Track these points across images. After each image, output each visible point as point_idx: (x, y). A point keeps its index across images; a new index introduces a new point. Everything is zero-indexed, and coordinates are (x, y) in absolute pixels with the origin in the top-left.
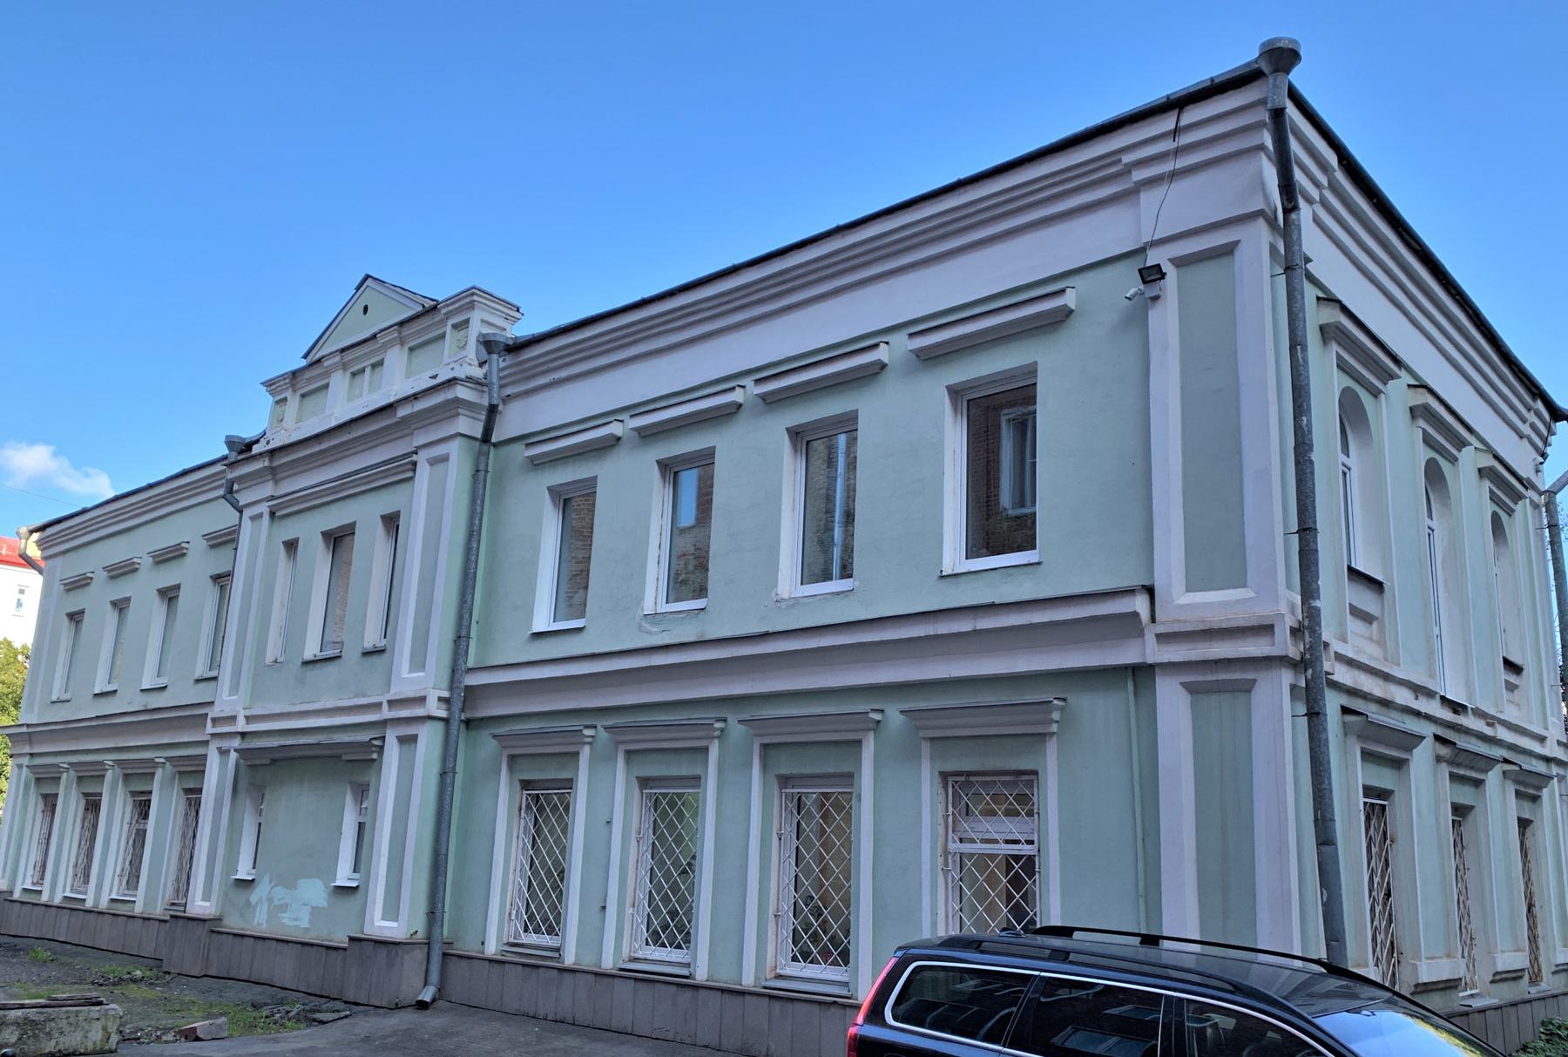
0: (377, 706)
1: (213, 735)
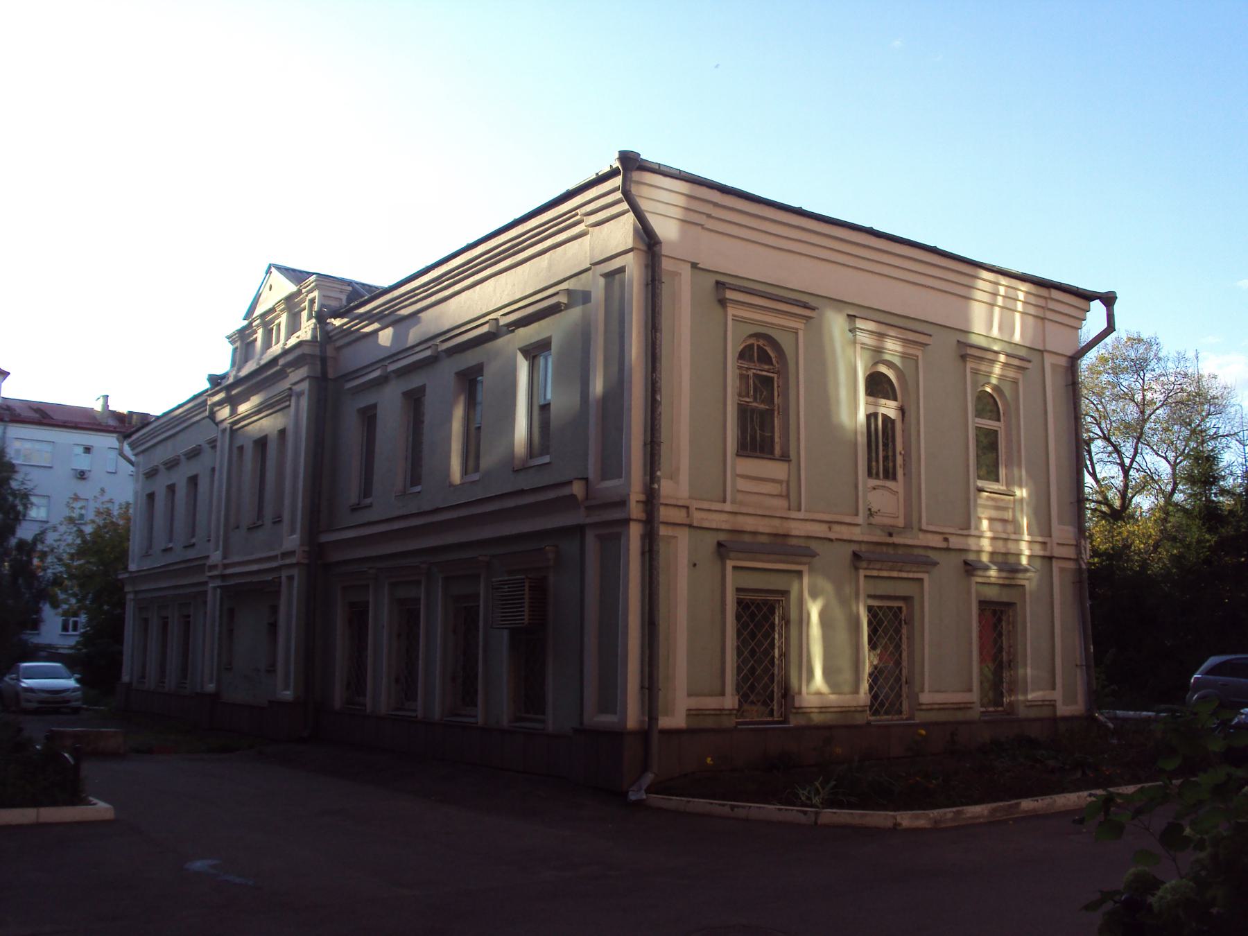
0: (274, 558)
1: (211, 577)
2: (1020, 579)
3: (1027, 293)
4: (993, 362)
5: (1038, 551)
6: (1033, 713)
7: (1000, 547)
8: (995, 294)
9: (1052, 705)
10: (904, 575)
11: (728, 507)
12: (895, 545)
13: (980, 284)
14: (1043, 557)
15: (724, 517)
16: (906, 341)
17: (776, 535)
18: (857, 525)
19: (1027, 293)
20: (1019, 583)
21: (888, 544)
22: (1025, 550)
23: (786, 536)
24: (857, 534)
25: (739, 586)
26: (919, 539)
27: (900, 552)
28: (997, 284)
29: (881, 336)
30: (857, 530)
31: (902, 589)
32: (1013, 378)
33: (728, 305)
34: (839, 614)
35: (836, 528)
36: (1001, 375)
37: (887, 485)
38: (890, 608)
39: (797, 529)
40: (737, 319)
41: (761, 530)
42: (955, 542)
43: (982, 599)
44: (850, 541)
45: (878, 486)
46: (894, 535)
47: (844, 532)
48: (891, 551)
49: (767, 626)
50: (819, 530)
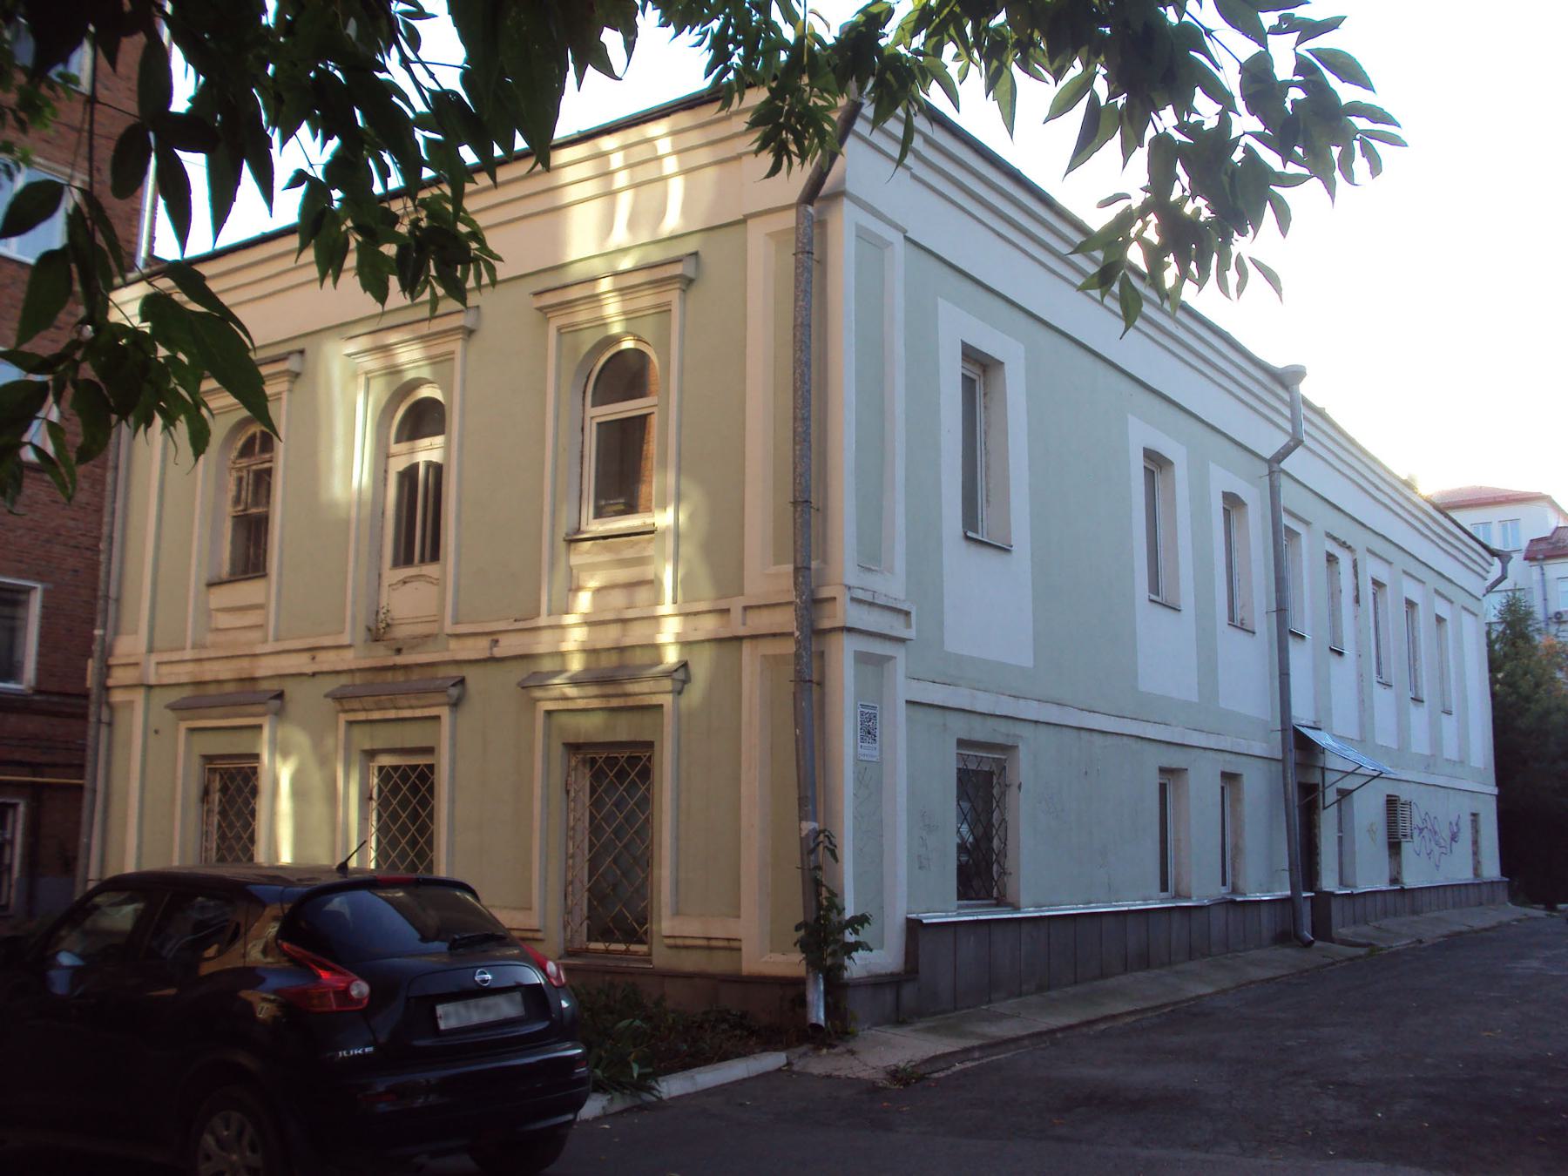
2: (596, 697)
3: (674, 133)
4: (595, 298)
5: (708, 626)
6: (690, 962)
7: (610, 636)
8: (607, 174)
9: (732, 947)
10: (407, 713)
11: (189, 654)
12: (406, 667)
13: (568, 175)
14: (719, 641)
15: (190, 667)
16: (422, 338)
17: (241, 680)
18: (349, 646)
19: (674, 133)
20: (646, 703)
21: (394, 668)
22: (669, 632)
23: (253, 679)
24: (348, 660)
25: (908, 699)
26: (448, 650)
27: (415, 676)
28: (602, 155)
29: (385, 349)
30: (349, 654)
31: (412, 736)
32: (386, 368)
33: (205, 399)
34: (316, 778)
35: (321, 656)
36: (624, 313)
37: (423, 572)
38: (414, 768)
39: (265, 668)
40: (438, 359)
41: (222, 676)
42: (509, 645)
43: (572, 740)
44: (337, 673)
45: (412, 577)
46: (404, 651)
47: (328, 661)
48: (400, 677)
49: (633, 774)
50: (300, 663)
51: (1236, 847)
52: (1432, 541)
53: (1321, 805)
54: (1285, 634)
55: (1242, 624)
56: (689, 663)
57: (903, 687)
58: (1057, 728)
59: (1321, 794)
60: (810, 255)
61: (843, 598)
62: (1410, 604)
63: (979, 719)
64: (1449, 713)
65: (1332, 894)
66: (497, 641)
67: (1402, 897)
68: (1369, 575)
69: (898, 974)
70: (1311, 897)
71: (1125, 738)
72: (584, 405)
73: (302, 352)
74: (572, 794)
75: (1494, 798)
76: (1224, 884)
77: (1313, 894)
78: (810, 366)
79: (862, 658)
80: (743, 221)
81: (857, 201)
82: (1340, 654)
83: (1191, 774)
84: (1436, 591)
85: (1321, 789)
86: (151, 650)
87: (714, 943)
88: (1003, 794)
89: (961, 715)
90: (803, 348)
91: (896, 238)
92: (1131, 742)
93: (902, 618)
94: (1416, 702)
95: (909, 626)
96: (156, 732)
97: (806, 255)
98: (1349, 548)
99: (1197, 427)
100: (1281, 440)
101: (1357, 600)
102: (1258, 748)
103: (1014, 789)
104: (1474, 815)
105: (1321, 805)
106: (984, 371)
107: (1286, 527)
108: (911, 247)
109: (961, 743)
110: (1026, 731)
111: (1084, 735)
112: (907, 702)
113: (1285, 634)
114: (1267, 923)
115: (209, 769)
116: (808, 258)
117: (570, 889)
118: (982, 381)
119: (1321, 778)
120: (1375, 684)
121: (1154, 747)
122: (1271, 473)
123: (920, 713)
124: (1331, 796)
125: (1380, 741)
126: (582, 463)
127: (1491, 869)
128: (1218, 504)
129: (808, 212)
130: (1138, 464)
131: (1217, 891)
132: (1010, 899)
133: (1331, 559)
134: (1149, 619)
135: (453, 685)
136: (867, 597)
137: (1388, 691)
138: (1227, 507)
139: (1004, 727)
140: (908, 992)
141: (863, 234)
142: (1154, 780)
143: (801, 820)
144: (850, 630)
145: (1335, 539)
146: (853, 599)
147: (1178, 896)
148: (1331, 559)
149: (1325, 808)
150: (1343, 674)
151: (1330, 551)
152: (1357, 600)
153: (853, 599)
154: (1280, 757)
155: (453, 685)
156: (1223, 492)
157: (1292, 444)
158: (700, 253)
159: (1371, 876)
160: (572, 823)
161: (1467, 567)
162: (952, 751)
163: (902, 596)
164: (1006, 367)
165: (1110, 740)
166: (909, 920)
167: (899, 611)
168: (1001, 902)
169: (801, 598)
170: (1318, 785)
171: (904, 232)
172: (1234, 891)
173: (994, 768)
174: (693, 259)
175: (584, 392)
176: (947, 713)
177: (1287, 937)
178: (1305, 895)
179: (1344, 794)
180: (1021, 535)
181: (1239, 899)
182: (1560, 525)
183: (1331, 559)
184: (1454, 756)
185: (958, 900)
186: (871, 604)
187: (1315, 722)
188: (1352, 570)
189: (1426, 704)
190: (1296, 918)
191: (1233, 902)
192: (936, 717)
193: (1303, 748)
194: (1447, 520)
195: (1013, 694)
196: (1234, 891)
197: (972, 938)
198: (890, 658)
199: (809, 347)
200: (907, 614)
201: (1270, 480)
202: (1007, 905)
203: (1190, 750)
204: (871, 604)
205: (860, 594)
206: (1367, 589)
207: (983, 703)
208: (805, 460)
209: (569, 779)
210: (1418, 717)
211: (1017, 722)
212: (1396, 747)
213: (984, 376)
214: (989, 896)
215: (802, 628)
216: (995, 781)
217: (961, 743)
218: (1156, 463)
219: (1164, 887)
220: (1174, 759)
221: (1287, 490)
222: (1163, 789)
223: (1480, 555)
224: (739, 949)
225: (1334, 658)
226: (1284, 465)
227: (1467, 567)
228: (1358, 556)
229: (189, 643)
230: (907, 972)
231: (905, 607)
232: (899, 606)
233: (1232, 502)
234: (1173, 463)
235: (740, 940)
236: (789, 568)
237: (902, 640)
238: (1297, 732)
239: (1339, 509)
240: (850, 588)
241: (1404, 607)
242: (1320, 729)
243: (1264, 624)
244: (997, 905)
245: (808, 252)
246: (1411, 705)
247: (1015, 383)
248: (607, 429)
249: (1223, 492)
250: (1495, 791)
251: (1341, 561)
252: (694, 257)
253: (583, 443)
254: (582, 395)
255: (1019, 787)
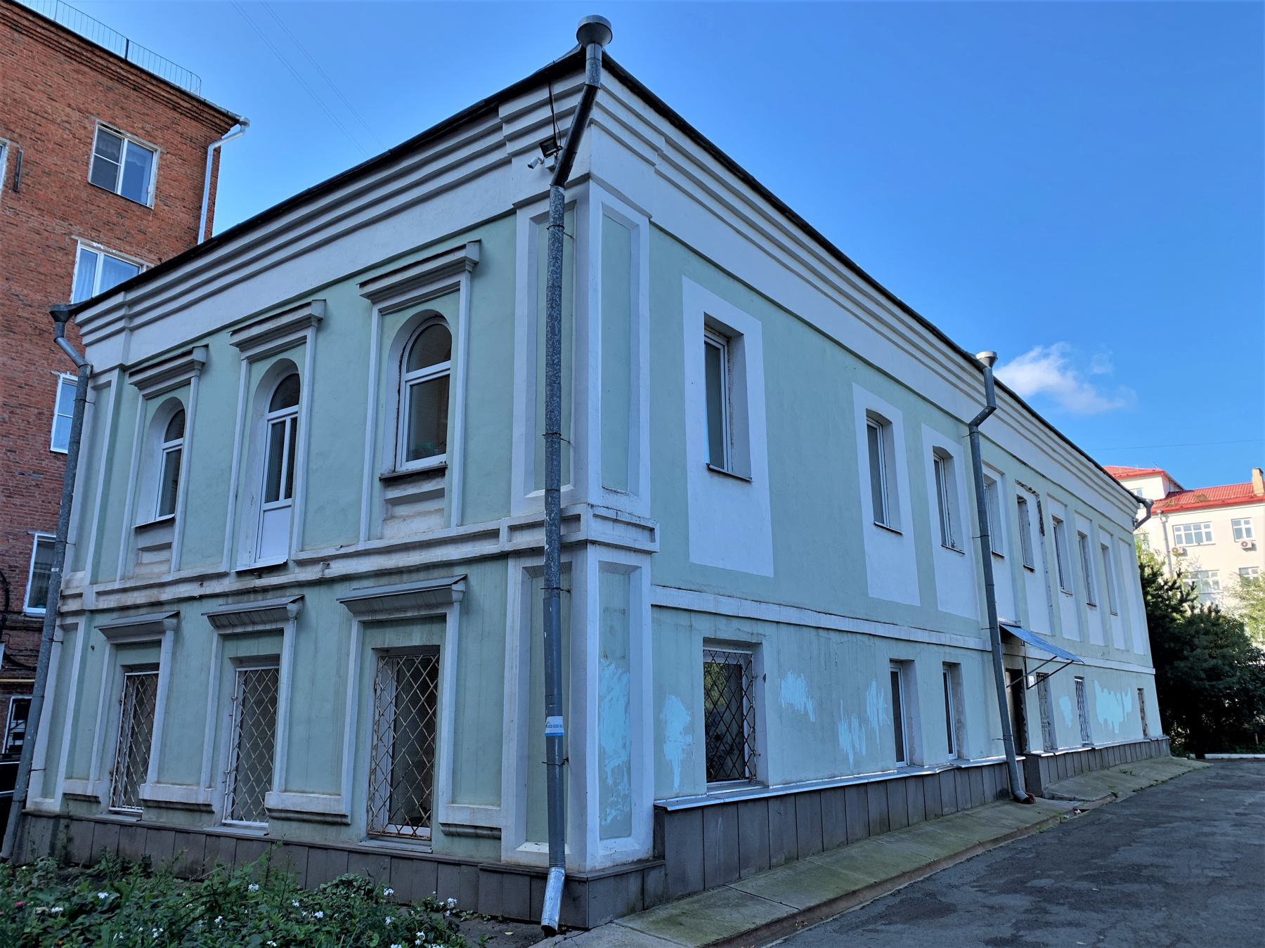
10: (261, 628)
51: (959, 721)
52: (1095, 490)
53: (1025, 687)
54: (987, 555)
55: (953, 546)
56: (469, 576)
57: (649, 594)
58: (798, 627)
59: (1025, 679)
60: (561, 228)
61: (587, 516)
62: (1083, 536)
63: (723, 621)
64: (1116, 614)
65: (1039, 756)
66: (329, 564)
67: (1095, 757)
68: (1049, 513)
69: (647, 860)
70: (1023, 760)
71: (859, 637)
72: (400, 371)
73: (206, 346)
74: (379, 692)
75: (1154, 677)
76: (951, 752)
77: (1024, 758)
78: (560, 321)
79: (608, 568)
80: (511, 213)
81: (602, 184)
82: (1032, 570)
83: (917, 664)
84: (1100, 527)
85: (1024, 674)
86: (94, 582)
87: (479, 831)
88: (750, 684)
89: (708, 617)
90: (554, 305)
91: (642, 222)
92: (865, 638)
93: (647, 533)
94: (1090, 607)
95: (653, 540)
96: (93, 648)
97: (557, 228)
98: (1034, 492)
99: (912, 397)
100: (977, 410)
101: (1042, 531)
102: (972, 643)
103: (760, 679)
104: (1139, 689)
105: (1025, 687)
106: (728, 342)
107: (985, 475)
108: (654, 229)
109: (707, 641)
110: (769, 630)
111: (821, 632)
112: (652, 605)
113: (987, 555)
114: (989, 785)
115: (128, 676)
116: (559, 230)
117: (373, 777)
118: (726, 349)
119: (1024, 665)
120: (1060, 594)
121: (885, 642)
122: (971, 434)
123: (666, 616)
124: (1032, 680)
125: (1066, 636)
126: (398, 418)
127: (1156, 730)
128: (930, 458)
129: (559, 192)
130: (862, 424)
131: (947, 760)
132: (760, 778)
133: (1020, 500)
134: (874, 540)
135: (293, 602)
136: (611, 514)
137: (1069, 598)
138: (937, 459)
139: (747, 627)
140: (654, 879)
141: (609, 214)
142: (887, 669)
143: (547, 715)
144: (594, 543)
145: (1023, 486)
146: (596, 516)
147: (912, 764)
148: (1021, 501)
149: (1028, 688)
150: (1034, 585)
151: (1021, 495)
152: (1042, 531)
153: (596, 516)
154: (991, 650)
155: (293, 602)
156: (933, 447)
157: (987, 411)
158: (483, 240)
159: (1068, 743)
160: (377, 717)
161: (1122, 510)
162: (699, 647)
163: (648, 516)
164: (745, 337)
165: (845, 637)
166: (656, 807)
167: (644, 527)
168: (752, 780)
169: (550, 516)
170: (1022, 670)
171: (650, 217)
172: (960, 757)
173: (742, 662)
174: (477, 245)
175: (401, 362)
176: (693, 615)
177: (1007, 795)
178: (1017, 759)
179: (1042, 678)
180: (759, 467)
181: (963, 766)
182: (1171, 491)
183: (1021, 501)
184: (1122, 647)
185: (707, 782)
186: (615, 521)
187: (1016, 622)
188: (1037, 510)
189: (1098, 608)
190: (1011, 778)
191: (959, 769)
192: (683, 619)
193: (1006, 638)
194: (1105, 475)
195: (756, 599)
196: (960, 757)
197: (720, 819)
198: (636, 568)
199: (560, 305)
200: (652, 530)
201: (971, 438)
202: (758, 783)
203: (917, 644)
204: (615, 521)
205: (604, 512)
206: (1049, 525)
207: (727, 607)
208: (555, 399)
209: (377, 679)
210: (1093, 617)
211: (759, 622)
212: (1078, 640)
213: (728, 346)
214: (742, 775)
215: (551, 542)
216: (743, 673)
217: (707, 641)
218: (878, 425)
219: (900, 757)
220: (902, 653)
221: (986, 450)
222: (894, 676)
223: (1128, 499)
224: (499, 838)
225: (1027, 573)
226: (981, 428)
227: (1122, 510)
228: (1041, 499)
229: (118, 578)
230: (655, 858)
231: (650, 525)
232: (643, 523)
233: (942, 457)
234: (891, 423)
235: (500, 829)
236: (542, 492)
237: (649, 553)
238: (1003, 630)
239: (1025, 464)
240: (592, 506)
241: (1078, 538)
242: (1020, 627)
243: (971, 547)
244: (750, 783)
245: (559, 226)
246: (1088, 608)
247: (753, 351)
248: (420, 389)
249: (933, 447)
250: (1154, 671)
251: (1029, 503)
252: (478, 243)
253: (399, 401)
254: (399, 364)
255: (764, 678)
